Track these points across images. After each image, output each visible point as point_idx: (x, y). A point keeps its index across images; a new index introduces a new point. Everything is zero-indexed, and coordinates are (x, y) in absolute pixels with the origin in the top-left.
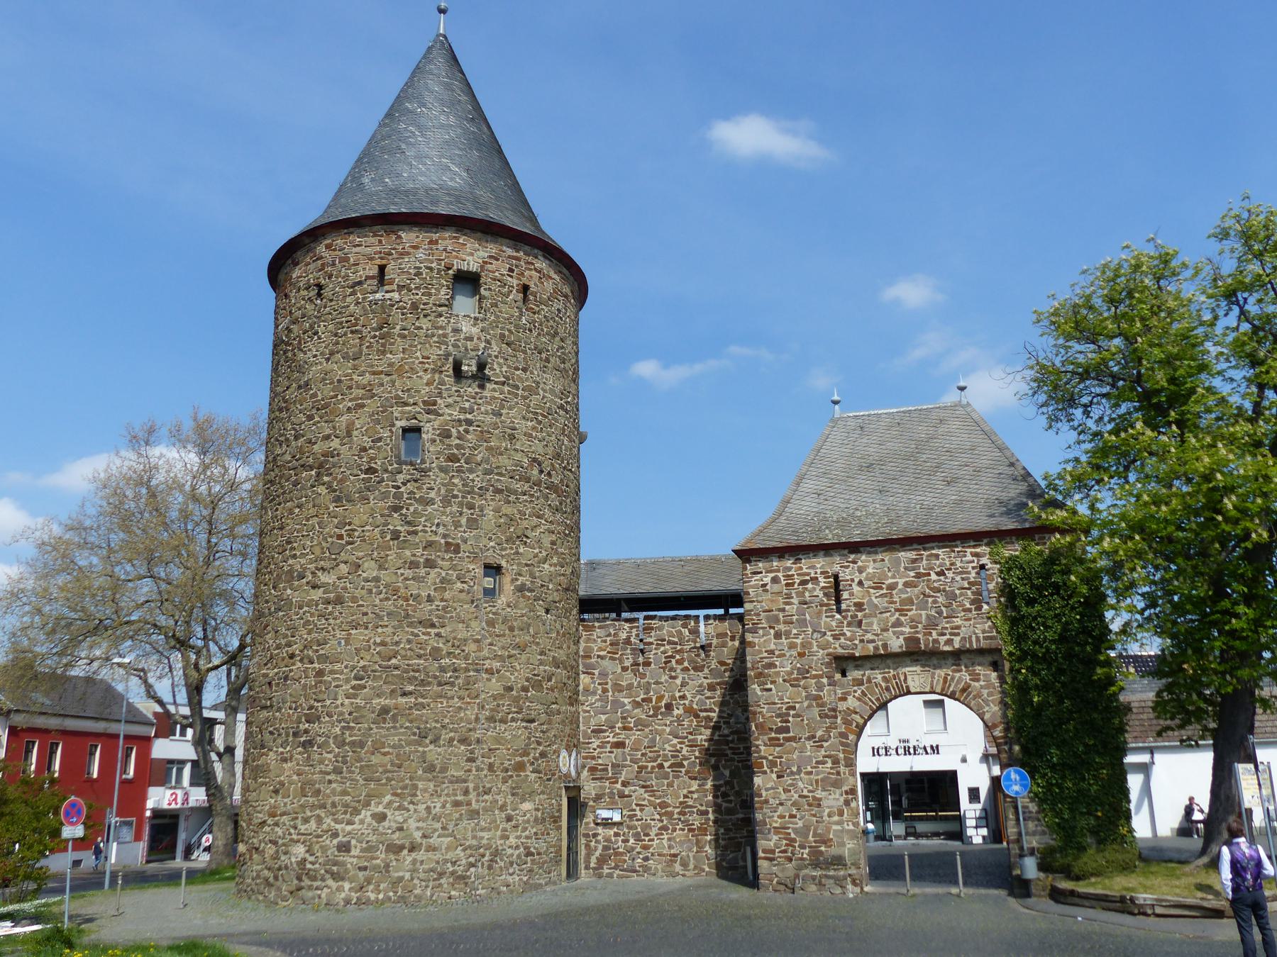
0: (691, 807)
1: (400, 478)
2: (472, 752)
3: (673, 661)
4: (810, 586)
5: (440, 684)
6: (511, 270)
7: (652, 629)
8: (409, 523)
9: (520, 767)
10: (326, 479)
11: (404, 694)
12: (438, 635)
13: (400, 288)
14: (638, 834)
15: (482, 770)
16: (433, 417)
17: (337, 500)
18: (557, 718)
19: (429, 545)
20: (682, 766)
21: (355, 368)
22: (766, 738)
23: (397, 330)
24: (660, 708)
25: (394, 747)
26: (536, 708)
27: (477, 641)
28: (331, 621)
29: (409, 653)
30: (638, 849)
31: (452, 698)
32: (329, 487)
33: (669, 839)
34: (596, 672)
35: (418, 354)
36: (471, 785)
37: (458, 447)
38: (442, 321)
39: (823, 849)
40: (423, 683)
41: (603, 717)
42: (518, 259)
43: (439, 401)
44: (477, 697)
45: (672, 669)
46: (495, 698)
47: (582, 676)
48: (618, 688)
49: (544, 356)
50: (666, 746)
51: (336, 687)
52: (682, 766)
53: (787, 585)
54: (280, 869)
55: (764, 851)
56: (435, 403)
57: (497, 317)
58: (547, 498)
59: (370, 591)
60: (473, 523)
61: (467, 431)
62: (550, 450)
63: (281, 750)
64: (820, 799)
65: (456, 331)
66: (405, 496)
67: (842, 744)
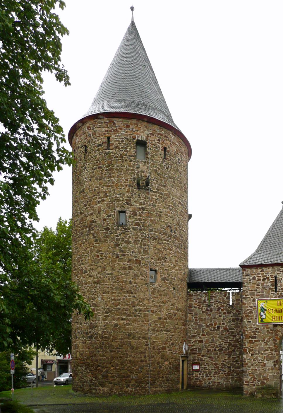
0: (225, 365)
1: (119, 232)
2: (147, 342)
3: (220, 310)
4: (266, 281)
5: (135, 316)
6: (159, 140)
7: (213, 297)
8: (122, 251)
9: (164, 348)
10: (92, 232)
11: (123, 319)
12: (134, 297)
13: (116, 148)
14: (207, 374)
15: (150, 349)
16: (130, 206)
17: (96, 241)
18: (178, 330)
19: (130, 261)
20: (222, 350)
21: (100, 184)
22: (248, 340)
23: (115, 167)
24: (215, 328)
25: (119, 339)
26: (169, 326)
27: (148, 300)
28: (96, 290)
29: (124, 304)
30: (207, 380)
31: (139, 321)
32: (93, 234)
33: (218, 377)
34: (193, 313)
35: (123, 178)
36: (147, 355)
37: (140, 219)
38: (132, 163)
39: (265, 382)
40: (129, 315)
41: (196, 331)
42: (161, 135)
43: (132, 199)
44: (148, 321)
45: (220, 313)
46: (155, 322)
47: (188, 315)
48: (201, 320)
49: (172, 180)
50: (217, 342)
51: (99, 316)
52: (222, 350)
53: (258, 280)
54: (84, 382)
55: (246, 382)
56: (130, 200)
57: (154, 162)
58: (173, 242)
59: (109, 279)
60: (146, 252)
61: (142, 213)
62: (175, 222)
63: (82, 339)
64: (265, 364)
65: (138, 168)
66: (120, 240)
67: (274, 343)
